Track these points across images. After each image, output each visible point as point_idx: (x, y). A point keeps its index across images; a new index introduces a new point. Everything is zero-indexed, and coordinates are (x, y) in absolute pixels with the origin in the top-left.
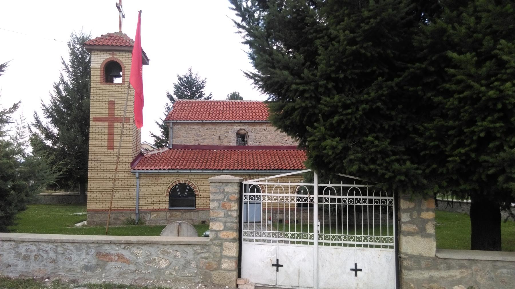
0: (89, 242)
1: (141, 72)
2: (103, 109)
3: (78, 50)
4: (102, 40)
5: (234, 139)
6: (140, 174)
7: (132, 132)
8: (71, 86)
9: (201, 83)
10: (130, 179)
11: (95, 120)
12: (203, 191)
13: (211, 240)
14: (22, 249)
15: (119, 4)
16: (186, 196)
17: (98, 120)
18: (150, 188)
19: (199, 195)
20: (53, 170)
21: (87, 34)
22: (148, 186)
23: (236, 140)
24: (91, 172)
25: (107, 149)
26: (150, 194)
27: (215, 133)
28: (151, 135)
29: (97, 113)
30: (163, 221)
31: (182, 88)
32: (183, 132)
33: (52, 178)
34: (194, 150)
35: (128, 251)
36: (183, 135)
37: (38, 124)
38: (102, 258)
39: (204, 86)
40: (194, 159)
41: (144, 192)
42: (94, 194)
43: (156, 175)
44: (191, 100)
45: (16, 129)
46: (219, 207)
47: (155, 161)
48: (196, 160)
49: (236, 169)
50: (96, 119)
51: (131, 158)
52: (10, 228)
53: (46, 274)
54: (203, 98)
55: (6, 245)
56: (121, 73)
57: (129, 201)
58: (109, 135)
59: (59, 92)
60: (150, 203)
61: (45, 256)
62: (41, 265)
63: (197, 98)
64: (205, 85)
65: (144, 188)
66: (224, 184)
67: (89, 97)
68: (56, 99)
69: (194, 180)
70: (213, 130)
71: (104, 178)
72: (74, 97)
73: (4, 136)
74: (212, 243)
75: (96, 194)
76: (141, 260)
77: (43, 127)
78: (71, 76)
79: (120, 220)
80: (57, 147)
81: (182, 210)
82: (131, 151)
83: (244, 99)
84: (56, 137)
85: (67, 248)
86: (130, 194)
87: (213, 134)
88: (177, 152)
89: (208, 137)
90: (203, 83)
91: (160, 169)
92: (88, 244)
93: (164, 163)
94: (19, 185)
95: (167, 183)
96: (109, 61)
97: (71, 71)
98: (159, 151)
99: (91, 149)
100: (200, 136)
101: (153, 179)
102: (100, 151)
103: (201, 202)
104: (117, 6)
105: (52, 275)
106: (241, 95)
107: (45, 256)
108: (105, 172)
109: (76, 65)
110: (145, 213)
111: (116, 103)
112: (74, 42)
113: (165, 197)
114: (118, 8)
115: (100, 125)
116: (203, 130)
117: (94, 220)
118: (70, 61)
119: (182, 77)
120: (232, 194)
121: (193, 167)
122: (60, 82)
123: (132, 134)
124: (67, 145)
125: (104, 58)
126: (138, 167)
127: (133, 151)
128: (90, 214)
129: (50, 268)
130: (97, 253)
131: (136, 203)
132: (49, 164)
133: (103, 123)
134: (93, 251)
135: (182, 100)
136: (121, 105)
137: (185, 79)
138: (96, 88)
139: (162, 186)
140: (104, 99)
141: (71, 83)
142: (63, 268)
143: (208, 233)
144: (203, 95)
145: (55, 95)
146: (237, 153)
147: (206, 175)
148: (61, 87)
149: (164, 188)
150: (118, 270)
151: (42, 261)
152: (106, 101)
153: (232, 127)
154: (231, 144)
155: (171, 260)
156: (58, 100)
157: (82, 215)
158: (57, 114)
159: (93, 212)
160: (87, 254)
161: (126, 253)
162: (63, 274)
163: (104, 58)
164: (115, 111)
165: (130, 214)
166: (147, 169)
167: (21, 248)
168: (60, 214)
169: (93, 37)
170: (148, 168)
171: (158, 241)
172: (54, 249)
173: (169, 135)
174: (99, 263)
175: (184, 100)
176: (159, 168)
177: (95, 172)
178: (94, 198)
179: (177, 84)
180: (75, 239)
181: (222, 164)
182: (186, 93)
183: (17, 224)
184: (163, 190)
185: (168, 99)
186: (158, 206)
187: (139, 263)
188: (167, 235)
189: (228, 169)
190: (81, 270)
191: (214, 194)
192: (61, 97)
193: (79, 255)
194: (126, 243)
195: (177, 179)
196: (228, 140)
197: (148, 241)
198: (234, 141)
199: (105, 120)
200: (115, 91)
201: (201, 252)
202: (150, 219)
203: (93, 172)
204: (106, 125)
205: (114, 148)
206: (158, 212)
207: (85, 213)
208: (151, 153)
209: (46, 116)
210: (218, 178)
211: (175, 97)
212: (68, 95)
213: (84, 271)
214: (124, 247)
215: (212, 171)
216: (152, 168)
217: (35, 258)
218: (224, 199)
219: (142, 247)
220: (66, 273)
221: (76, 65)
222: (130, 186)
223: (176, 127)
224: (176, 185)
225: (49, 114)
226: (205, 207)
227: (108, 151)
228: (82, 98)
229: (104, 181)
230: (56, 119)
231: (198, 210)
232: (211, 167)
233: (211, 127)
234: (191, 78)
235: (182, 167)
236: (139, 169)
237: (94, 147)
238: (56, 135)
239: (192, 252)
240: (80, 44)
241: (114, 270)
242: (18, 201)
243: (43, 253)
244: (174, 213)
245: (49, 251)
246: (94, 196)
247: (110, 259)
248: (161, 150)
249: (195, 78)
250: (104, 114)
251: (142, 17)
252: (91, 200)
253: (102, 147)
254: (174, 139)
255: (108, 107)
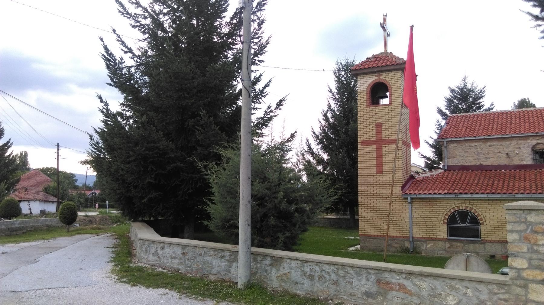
0: (368, 267)
1: (415, 89)
2: (370, 132)
3: (343, 76)
4: (368, 63)
5: (528, 156)
6: (412, 199)
7: (401, 154)
8: (338, 113)
9: (479, 93)
10: (402, 204)
11: (363, 143)
12: (490, 220)
13: (511, 279)
14: (307, 268)
15: (384, 23)
16: (468, 225)
17: (366, 143)
18: (424, 214)
19: (485, 224)
20: (330, 194)
21: (351, 60)
22: (421, 212)
23: (531, 157)
24: (361, 196)
25: (376, 173)
26: (424, 220)
27: (502, 149)
28: (421, 156)
29: (365, 136)
30: (442, 252)
31: (455, 101)
32: (460, 151)
33: (328, 202)
34: (475, 171)
35: (409, 282)
36: (460, 154)
37: (311, 151)
38: (382, 286)
39: (483, 96)
40: (476, 182)
41: (418, 218)
42: (365, 219)
43: (430, 200)
44: (467, 114)
45: (297, 157)
46: (520, 240)
47: (428, 184)
48: (478, 182)
49: (534, 193)
50: (364, 143)
51: (402, 182)
52: (295, 247)
53: (329, 296)
54: (482, 110)
55: (294, 263)
56: (388, 94)
57: (402, 228)
58: (377, 158)
59: (327, 119)
60: (425, 230)
61: (328, 277)
62: (324, 286)
63: (475, 111)
64: (484, 95)
65: (418, 214)
66: (526, 212)
67: (356, 121)
68: (325, 126)
69: (477, 206)
70: (498, 147)
71: (374, 202)
72: (341, 123)
73: (288, 163)
74: (513, 282)
75: (367, 219)
76: (425, 293)
77: (314, 153)
78: (337, 103)
79: (394, 247)
80: (327, 171)
81: (464, 240)
82: (401, 174)
83: (537, 106)
84: (325, 163)
85: (348, 272)
86: (403, 220)
87: (498, 151)
88: (453, 174)
89: (492, 155)
90: (482, 92)
91: (435, 194)
92: (367, 270)
93: (439, 187)
94: (301, 208)
95: (444, 209)
96: (375, 83)
97: (338, 97)
98: (432, 174)
99: (360, 173)
100: (482, 154)
101: (426, 204)
102: (369, 175)
103: (488, 232)
104: (381, 26)
105: (335, 297)
106: (532, 101)
107: (328, 277)
108: (375, 196)
109: (342, 92)
110: (420, 241)
111: (383, 124)
112: (339, 70)
113: (442, 225)
114: (383, 27)
115: (368, 148)
116: (485, 147)
117: (367, 245)
118: (336, 89)
119: (455, 88)
120: (538, 225)
121: (474, 191)
122: (327, 110)
123: (401, 156)
124: (336, 169)
125: (370, 80)
126: (410, 191)
127: (403, 174)
128: (362, 239)
129: (332, 290)
130: (377, 280)
131: (409, 230)
132: (325, 188)
133: (371, 146)
134: (373, 278)
135: (456, 115)
136: (388, 126)
137: (459, 90)
138: (363, 112)
139: (437, 213)
140: (371, 122)
141: (338, 109)
142: (345, 291)
143: (505, 270)
144: (482, 106)
145: (323, 122)
146: (534, 173)
147: (492, 200)
148: (329, 115)
149: (440, 215)
150: (399, 301)
151: (325, 282)
152: (374, 123)
153: (525, 141)
154: (525, 163)
155: (461, 297)
156: (326, 127)
157: (354, 239)
158: (326, 140)
159: (365, 237)
160: (368, 280)
161: (407, 284)
162: (345, 297)
163: (370, 80)
164: (383, 133)
165: (404, 242)
166: (420, 194)
167: (306, 267)
168: (333, 236)
169: (357, 62)
170: (421, 192)
171: (443, 274)
172: (335, 271)
173: (443, 155)
174: (380, 291)
175: (459, 115)
176: (434, 192)
177: (365, 196)
178: (366, 222)
179: (448, 97)
180: (355, 263)
181: (514, 188)
182: (460, 106)
183: (300, 244)
184: (440, 217)
185: (439, 115)
186: (434, 235)
187: (422, 296)
188: (453, 269)
189: (522, 193)
190: (362, 296)
191: (513, 224)
192: (329, 124)
193: (360, 280)
194: (407, 273)
195: (455, 204)
196: (520, 158)
197: (433, 273)
198: (529, 159)
199: (373, 143)
200: (382, 112)
201: (498, 292)
202: (427, 248)
203: (363, 196)
204: (374, 148)
205: (383, 171)
206: (435, 242)
207: (357, 237)
208: (423, 175)
209: (317, 143)
210: (516, 205)
211: (447, 112)
212: (335, 121)
213: (365, 297)
214: (406, 277)
215: (501, 196)
216: (426, 192)
217: (319, 278)
218: (527, 230)
219: (425, 279)
220: (348, 297)
221: (342, 92)
222: (401, 212)
223: (452, 146)
224: (455, 211)
225: (319, 141)
226: (493, 239)
227: (377, 174)
228: (348, 123)
229: (375, 206)
230: (325, 145)
231: (484, 242)
232: (499, 191)
233: (496, 143)
234: (466, 88)
235: (461, 191)
236: (410, 194)
237: (363, 171)
238: (325, 160)
239: (486, 291)
240: (345, 71)
241: (396, 300)
242: (301, 223)
243: (326, 274)
244: (454, 243)
245: (331, 273)
246: (365, 220)
247: (391, 288)
248: (434, 173)
249: (470, 88)
250: (372, 137)
251: (414, 32)
252: (363, 224)
253: (371, 171)
254: (449, 160)
255: (375, 130)
